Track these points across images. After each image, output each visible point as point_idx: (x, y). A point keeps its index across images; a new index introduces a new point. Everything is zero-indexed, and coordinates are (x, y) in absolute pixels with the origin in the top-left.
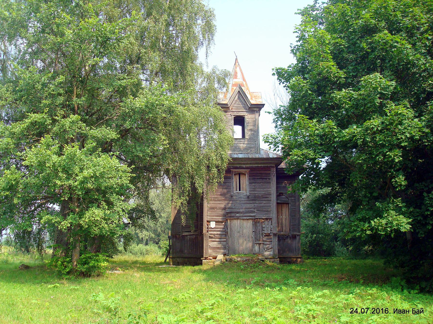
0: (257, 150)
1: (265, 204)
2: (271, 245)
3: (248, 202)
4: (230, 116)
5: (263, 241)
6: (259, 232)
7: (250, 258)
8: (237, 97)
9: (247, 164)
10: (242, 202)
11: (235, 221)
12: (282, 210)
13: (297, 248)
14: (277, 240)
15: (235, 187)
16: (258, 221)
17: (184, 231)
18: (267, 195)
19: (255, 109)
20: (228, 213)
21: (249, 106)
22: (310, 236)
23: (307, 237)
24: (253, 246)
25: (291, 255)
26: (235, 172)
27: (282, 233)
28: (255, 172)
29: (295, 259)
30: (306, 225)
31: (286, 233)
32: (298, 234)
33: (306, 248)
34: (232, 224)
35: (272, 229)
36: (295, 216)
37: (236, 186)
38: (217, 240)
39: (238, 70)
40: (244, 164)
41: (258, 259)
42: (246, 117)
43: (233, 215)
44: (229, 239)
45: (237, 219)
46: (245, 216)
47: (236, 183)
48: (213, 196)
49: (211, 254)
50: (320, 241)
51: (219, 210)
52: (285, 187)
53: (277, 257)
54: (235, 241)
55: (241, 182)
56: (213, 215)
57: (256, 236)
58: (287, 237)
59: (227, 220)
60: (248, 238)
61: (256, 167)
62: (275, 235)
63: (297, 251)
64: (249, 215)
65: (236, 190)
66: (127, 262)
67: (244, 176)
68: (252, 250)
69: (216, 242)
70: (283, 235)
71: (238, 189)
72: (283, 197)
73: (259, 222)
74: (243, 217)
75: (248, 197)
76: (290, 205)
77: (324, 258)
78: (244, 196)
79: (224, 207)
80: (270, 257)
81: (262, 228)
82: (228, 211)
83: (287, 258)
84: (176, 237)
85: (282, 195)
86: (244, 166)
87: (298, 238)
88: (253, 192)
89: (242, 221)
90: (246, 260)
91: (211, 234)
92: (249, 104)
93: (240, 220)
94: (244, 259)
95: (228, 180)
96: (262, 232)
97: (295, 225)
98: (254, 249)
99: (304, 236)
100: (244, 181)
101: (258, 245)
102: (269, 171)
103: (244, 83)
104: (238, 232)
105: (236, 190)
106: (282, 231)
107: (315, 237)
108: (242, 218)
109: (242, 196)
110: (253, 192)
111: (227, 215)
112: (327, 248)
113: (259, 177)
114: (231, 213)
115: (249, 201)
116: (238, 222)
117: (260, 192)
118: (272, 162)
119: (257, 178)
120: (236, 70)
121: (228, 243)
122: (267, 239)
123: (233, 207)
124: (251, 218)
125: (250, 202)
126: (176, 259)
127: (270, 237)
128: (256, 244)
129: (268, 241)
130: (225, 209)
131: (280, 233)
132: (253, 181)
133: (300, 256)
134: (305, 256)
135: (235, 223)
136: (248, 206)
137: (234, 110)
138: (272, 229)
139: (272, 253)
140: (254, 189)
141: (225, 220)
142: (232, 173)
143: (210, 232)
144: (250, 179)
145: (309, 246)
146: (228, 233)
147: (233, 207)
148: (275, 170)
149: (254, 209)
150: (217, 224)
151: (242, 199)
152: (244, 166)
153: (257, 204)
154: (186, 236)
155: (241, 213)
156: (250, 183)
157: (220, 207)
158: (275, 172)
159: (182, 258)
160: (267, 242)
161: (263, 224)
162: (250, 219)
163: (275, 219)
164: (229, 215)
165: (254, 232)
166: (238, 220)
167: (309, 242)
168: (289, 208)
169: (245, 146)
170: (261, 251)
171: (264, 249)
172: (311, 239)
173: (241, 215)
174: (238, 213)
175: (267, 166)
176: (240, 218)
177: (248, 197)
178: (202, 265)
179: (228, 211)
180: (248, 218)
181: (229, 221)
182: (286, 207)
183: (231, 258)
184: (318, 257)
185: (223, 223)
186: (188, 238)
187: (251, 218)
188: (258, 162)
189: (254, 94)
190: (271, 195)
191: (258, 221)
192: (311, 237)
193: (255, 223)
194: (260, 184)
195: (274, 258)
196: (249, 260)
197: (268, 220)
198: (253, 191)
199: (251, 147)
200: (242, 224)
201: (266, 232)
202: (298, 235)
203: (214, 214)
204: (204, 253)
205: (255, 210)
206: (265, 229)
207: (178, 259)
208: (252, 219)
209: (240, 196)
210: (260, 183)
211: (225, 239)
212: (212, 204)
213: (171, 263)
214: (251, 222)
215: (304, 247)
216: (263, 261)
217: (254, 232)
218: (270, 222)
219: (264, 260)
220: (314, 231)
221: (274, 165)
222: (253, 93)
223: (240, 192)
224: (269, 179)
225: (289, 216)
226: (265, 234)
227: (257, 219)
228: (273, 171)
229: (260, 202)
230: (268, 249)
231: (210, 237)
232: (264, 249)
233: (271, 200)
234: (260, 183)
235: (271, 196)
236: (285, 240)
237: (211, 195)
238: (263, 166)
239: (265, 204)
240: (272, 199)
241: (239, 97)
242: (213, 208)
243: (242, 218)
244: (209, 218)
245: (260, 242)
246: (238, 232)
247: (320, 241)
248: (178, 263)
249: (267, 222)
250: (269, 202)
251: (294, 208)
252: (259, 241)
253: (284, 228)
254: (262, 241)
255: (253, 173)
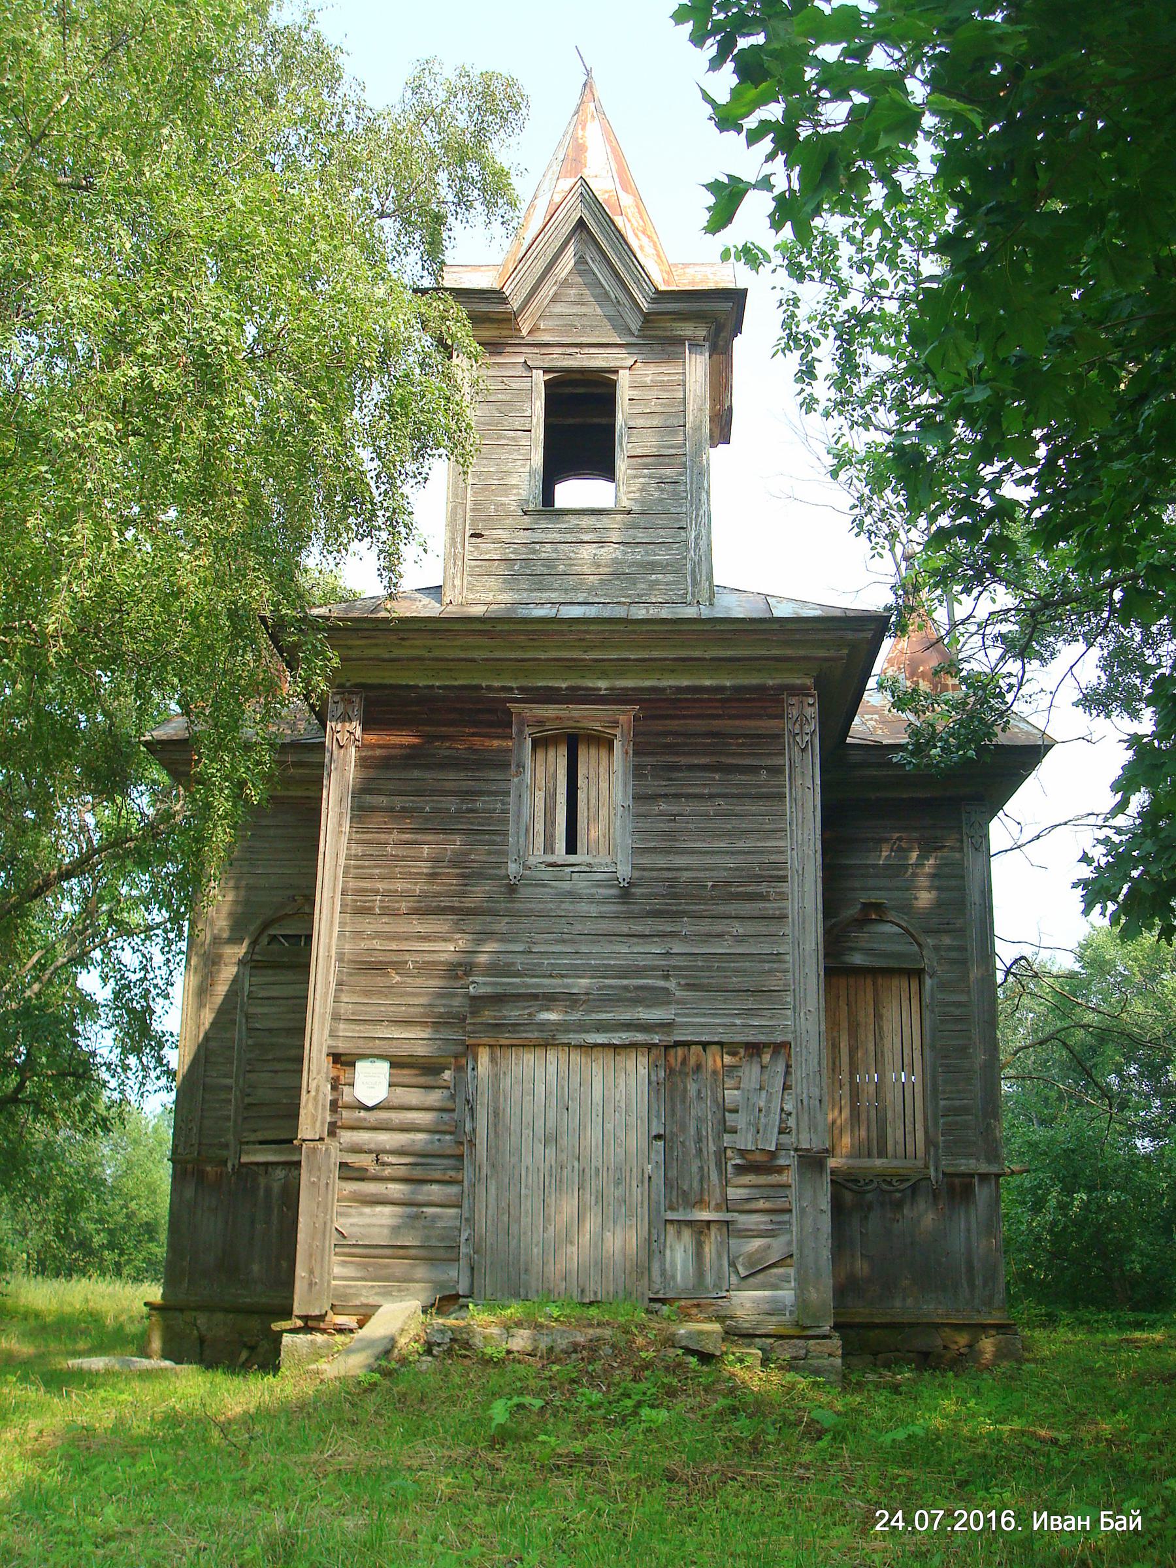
0: (695, 583)
1: (740, 939)
2: (783, 1239)
3: (625, 929)
4: (520, 371)
5: (726, 1205)
6: (699, 1139)
7: (608, 1332)
8: (568, 261)
9: (622, 667)
10: (578, 927)
11: (529, 1057)
12: (878, 1016)
13: (977, 1264)
14: (825, 1203)
15: (540, 827)
16: (692, 1061)
17: (253, 1137)
18: (759, 879)
19: (687, 330)
20: (478, 1003)
21: (645, 305)
22: (1053, 1202)
23: (1038, 1206)
24: (653, 1248)
25: (932, 1309)
26: (540, 722)
27: (878, 1162)
28: (673, 725)
29: (962, 1339)
30: (1033, 1145)
31: (909, 1163)
32: (984, 1168)
33: (1038, 1265)
34: (506, 1083)
35: (791, 1122)
36: (963, 1051)
37: (550, 822)
38: (395, 1190)
39: (593, 134)
40: (599, 668)
41: (670, 1341)
42: (624, 380)
43: (513, 1013)
44: (481, 1190)
45: (546, 1046)
46: (601, 1027)
47: (551, 797)
48: (380, 886)
49: (345, 1297)
50: (1109, 1230)
51: (419, 981)
52: (896, 870)
53: (826, 1329)
54: (526, 1205)
55: (581, 795)
56: (373, 1012)
57: (673, 1173)
58: (914, 1188)
59: (470, 1050)
60: (618, 1183)
61: (679, 689)
62: (812, 1162)
63: (979, 1282)
64: (626, 1015)
65: (549, 848)
66: (95, 1317)
67: (604, 753)
68: (642, 1270)
69: (387, 1209)
70: (886, 1177)
71: (561, 844)
72: (888, 928)
73: (698, 1067)
74: (582, 1028)
75: (625, 894)
76: (928, 982)
77: (1131, 1317)
78: (599, 884)
79: (455, 958)
80: (771, 1325)
81: (725, 1110)
82: (480, 985)
83: (912, 1325)
84: (201, 1176)
85: (881, 921)
86: (602, 684)
87: (982, 1193)
88: (661, 861)
89: (576, 1057)
90: (575, 1348)
91: (356, 1150)
92: (641, 291)
93: (563, 1056)
94: (562, 1343)
95: (492, 775)
96: (719, 1137)
97: (965, 1110)
98: (656, 1267)
99: (1024, 1203)
100: (604, 785)
101: (687, 1234)
102: (772, 717)
103: (626, 200)
104: (551, 1139)
105: (549, 848)
106: (882, 1153)
107: (1085, 1206)
108: (575, 1038)
109: (581, 884)
110: (661, 861)
111: (474, 1013)
112: (1146, 1261)
113: (703, 761)
114: (499, 999)
115: (629, 917)
116: (552, 1069)
117: (708, 860)
118: (789, 652)
119: (691, 768)
120: (580, 133)
121: (470, 1221)
122: (755, 1192)
123: (519, 959)
124: (640, 1037)
125: (638, 928)
126: (189, 1316)
127: (774, 1179)
128: (671, 1229)
129: (761, 1204)
130: (460, 970)
131: (866, 1162)
132: (653, 786)
133: (996, 1318)
134: (1030, 1308)
135: (528, 1071)
136: (623, 952)
137: (547, 338)
138: (791, 1122)
139: (787, 1295)
140: (671, 835)
141: (460, 1048)
142: (521, 732)
143: (347, 1137)
144: (638, 772)
145: (1054, 1256)
146: (472, 1144)
147: (519, 962)
148: (812, 712)
149: (666, 977)
150: (406, 1075)
151: (584, 907)
152: (602, 684)
153: (685, 939)
154: (262, 1169)
155: (571, 1000)
156: (637, 798)
157: (428, 958)
158: (813, 726)
159: (226, 1311)
160: (756, 1218)
161: (729, 1083)
162: (634, 1046)
163: (814, 1045)
164: (488, 1015)
165: (658, 1137)
166: (552, 1055)
167: (1050, 1232)
168: (927, 999)
169: (608, 553)
170: (709, 1279)
171: (732, 1264)
172: (1065, 1215)
173: (575, 1016)
174: (549, 1000)
175: (762, 688)
176: (564, 1038)
177: (625, 894)
178: (276, 1369)
179: (482, 990)
180: (617, 1038)
181: (484, 1057)
182: (905, 996)
183: (460, 1330)
184: (1099, 1311)
185: (447, 1075)
186: (276, 1187)
187: (640, 1037)
188: (697, 653)
189: (690, 271)
190: (783, 879)
191: (692, 1061)
192: (1063, 1207)
193: (671, 1072)
194: (709, 808)
195: (802, 1331)
196: (593, 1347)
197: (766, 1058)
198: (666, 851)
199: (651, 567)
200: (575, 1079)
201: (745, 1141)
202: (984, 1177)
203: (386, 1005)
204: (300, 1287)
205: (672, 984)
206: (739, 1120)
207: (202, 1320)
208: (650, 1047)
209: (566, 886)
210: (712, 796)
211: (453, 1190)
212: (371, 937)
213: (156, 1344)
214: (643, 1072)
215: (1026, 1261)
216: (706, 1358)
217: (658, 1137)
218: (780, 1067)
219: (710, 1348)
220: (1075, 1176)
221: (809, 682)
222: (686, 265)
223: (572, 859)
224: (777, 770)
225: (927, 1051)
226: (742, 1153)
227: (687, 1044)
228: (802, 720)
229: (705, 927)
230: (757, 1271)
231: (349, 1172)
232: (732, 1264)
233: (783, 917)
234: (712, 796)
235: (784, 887)
236: (898, 1205)
237: (371, 877)
238: (736, 689)
239: (740, 939)
240: (791, 908)
241: (581, 261)
242: (376, 967)
243: (575, 1038)
244: (348, 1037)
245: (705, 1215)
246: (551, 1139)
247: (1109, 1230)
248: (202, 1340)
249: (756, 1069)
250: (773, 929)
251: (959, 1004)
252: (700, 1203)
253: (895, 1134)
254: (718, 1208)
255: (658, 734)
